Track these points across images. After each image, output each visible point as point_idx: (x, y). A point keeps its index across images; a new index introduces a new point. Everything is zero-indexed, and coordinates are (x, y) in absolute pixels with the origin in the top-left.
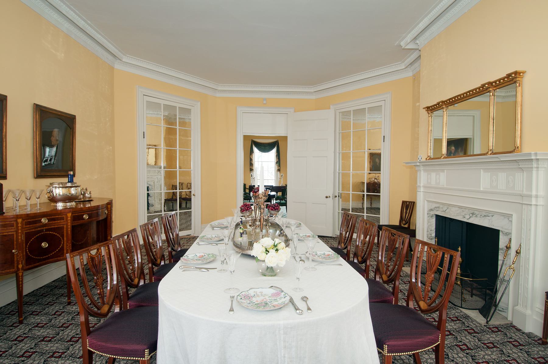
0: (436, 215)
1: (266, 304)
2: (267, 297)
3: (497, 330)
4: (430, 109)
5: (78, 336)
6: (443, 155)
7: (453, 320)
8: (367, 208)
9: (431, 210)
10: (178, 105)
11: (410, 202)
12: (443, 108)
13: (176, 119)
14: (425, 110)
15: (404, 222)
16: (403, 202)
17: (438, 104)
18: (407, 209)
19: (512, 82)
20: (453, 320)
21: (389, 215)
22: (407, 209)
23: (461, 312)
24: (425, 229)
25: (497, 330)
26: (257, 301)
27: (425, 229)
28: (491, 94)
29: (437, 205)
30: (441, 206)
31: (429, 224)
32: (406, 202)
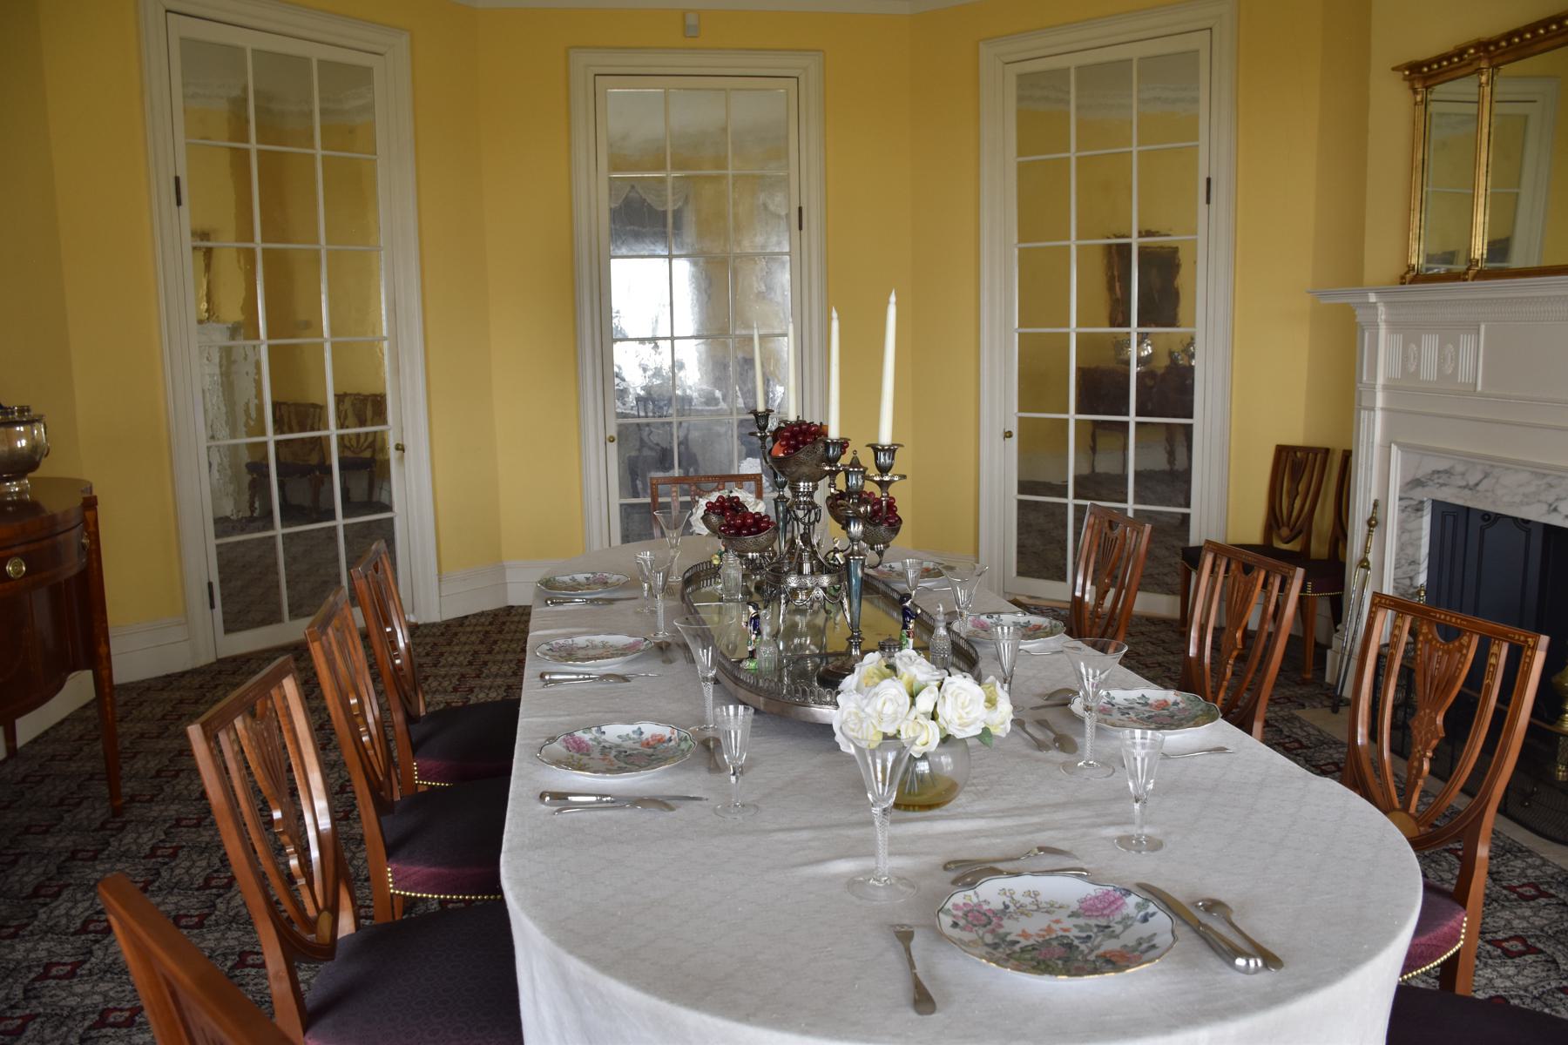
0: (1436, 504)
1: (1070, 946)
2: (1062, 915)
3: (1533, 892)
4: (1423, 74)
5: (41, 900)
6: (1471, 262)
7: (1523, 897)
8: (1137, 474)
9: (1417, 483)
10: (316, 53)
11: (1306, 450)
12: (1479, 71)
13: (310, 114)
14: (1399, 75)
15: (1285, 532)
16: (1283, 452)
17: (1461, 52)
18: (1296, 479)
19: (1471, 69)
20: (1523, 897)
21: (1227, 499)
22: (1296, 479)
23: (1545, 862)
24: (1391, 553)
25: (1533, 892)
26: (1025, 935)
27: (1391, 553)
28: (1484, 79)
29: (1442, 465)
30: (1460, 468)
31: (1406, 537)
32: (1294, 449)
